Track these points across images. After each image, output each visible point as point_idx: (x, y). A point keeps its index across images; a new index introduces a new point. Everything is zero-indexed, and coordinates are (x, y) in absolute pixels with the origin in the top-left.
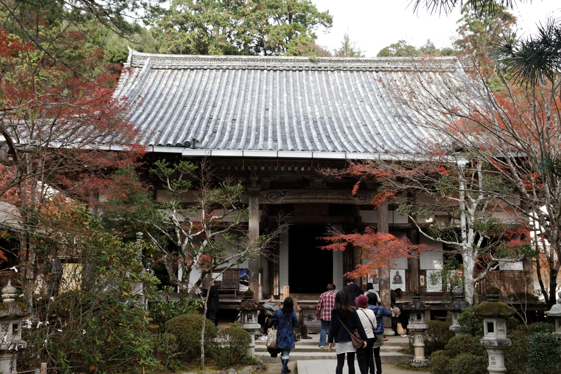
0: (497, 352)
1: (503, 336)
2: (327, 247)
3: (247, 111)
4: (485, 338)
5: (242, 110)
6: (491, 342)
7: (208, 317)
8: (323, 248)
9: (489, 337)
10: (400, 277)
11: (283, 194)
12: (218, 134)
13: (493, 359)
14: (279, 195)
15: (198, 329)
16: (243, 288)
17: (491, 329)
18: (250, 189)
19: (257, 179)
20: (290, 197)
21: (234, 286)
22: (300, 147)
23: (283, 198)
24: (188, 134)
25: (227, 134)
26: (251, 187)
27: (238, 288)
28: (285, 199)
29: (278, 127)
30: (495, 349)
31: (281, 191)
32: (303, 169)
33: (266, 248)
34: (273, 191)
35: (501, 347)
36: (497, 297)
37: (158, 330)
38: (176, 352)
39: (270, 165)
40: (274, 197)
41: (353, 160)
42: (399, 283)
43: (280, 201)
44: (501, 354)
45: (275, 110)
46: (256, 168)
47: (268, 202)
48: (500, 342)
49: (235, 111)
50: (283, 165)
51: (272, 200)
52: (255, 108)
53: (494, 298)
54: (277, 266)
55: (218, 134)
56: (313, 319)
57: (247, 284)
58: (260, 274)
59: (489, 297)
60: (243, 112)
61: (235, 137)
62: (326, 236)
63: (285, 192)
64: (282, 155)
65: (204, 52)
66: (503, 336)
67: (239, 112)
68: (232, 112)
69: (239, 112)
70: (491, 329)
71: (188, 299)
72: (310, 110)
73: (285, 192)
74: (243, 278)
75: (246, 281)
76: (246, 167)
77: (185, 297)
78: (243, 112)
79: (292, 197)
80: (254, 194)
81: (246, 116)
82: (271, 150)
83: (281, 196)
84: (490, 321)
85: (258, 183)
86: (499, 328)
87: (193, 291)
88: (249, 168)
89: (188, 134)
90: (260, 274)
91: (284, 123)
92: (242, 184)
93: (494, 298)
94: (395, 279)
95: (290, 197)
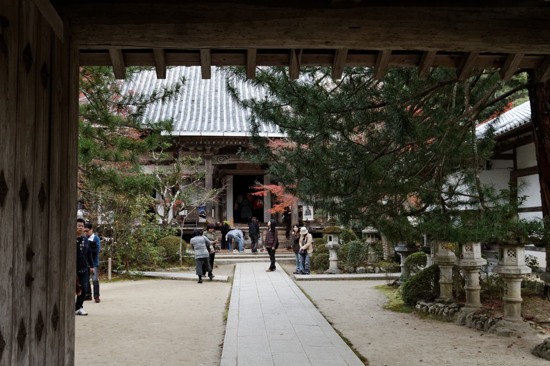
0: (333, 251)
1: (336, 243)
2: (256, 193)
3: (202, 94)
4: (328, 244)
5: (199, 91)
6: (330, 246)
7: (183, 238)
8: (253, 194)
9: (330, 244)
10: (310, 211)
11: (228, 158)
12: (182, 114)
13: (331, 254)
14: (225, 158)
15: (177, 245)
16: (201, 220)
17: (330, 240)
18: (206, 155)
19: (210, 148)
20: (232, 159)
21: (195, 219)
22: (239, 129)
23: (228, 160)
24: (161, 114)
25: (189, 114)
26: (206, 153)
27: (198, 220)
28: (229, 161)
29: (224, 108)
30: (332, 249)
31: (226, 156)
32: (240, 143)
33: (216, 198)
34: (220, 156)
35: (335, 248)
36: (335, 224)
37: (114, 259)
38: (166, 257)
39: (218, 141)
40: (222, 160)
41: (271, 138)
42: (309, 215)
43: (226, 162)
44: (335, 252)
45: (222, 92)
46: (209, 143)
47: (218, 163)
48: (334, 246)
49: (193, 93)
50: (227, 141)
51: (220, 162)
52: (208, 90)
53: (333, 224)
54: (225, 204)
55: (182, 114)
56: (248, 239)
57: (204, 217)
58: (213, 210)
59: (331, 224)
60: (199, 94)
61: (194, 117)
62: (255, 186)
63: (229, 156)
64: (226, 134)
65: (205, 179)
66: (336, 243)
67: (196, 94)
68: (191, 94)
69: (196, 94)
70: (330, 240)
71: (168, 227)
72: (248, 92)
73: (229, 156)
74: (201, 213)
75: (203, 215)
76: (203, 142)
77: (166, 226)
78: (199, 94)
79: (234, 160)
80: (208, 158)
81: (202, 98)
82: (219, 131)
83: (227, 159)
84: (330, 235)
85: (211, 150)
86: (334, 239)
87: (171, 223)
88: (205, 143)
89: (161, 114)
90: (213, 210)
91: (229, 104)
92: (201, 157)
93: (333, 224)
94: (306, 212)
95: (232, 159)
